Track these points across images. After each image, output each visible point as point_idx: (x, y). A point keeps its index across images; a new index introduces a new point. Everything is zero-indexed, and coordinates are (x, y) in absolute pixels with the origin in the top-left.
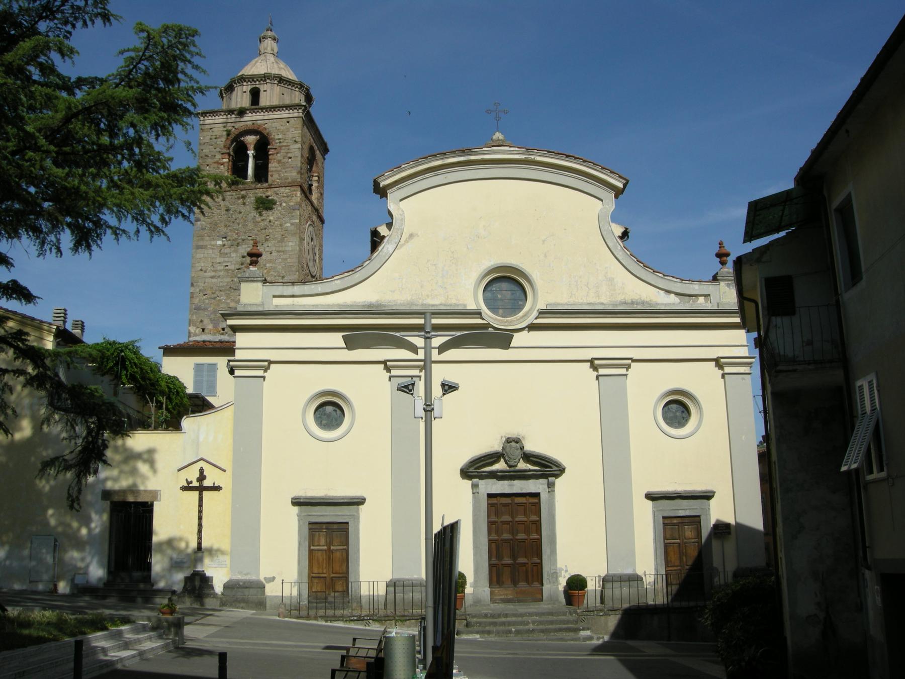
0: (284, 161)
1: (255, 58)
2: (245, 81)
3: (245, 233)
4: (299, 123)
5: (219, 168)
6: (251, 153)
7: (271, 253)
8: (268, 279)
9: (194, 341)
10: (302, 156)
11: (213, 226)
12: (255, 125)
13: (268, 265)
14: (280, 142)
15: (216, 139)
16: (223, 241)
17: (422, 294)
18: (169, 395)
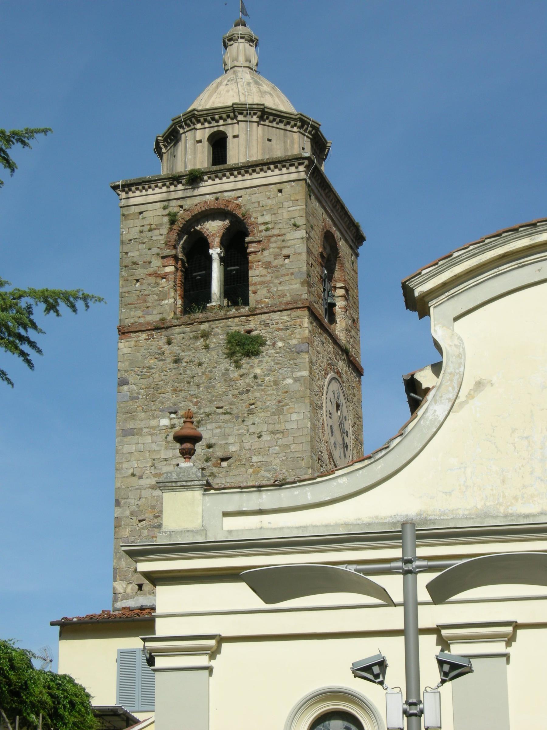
0: (275, 263)
1: (217, 77)
2: (199, 121)
3: (211, 402)
4: (300, 190)
5: (157, 284)
6: (215, 252)
7: (260, 437)
8: (215, 482)
9: (124, 608)
10: (309, 252)
11: (152, 391)
12: (220, 201)
13: (255, 459)
14: (267, 230)
15: (150, 230)
16: (171, 419)
17: (504, 496)
18: (56, 709)
